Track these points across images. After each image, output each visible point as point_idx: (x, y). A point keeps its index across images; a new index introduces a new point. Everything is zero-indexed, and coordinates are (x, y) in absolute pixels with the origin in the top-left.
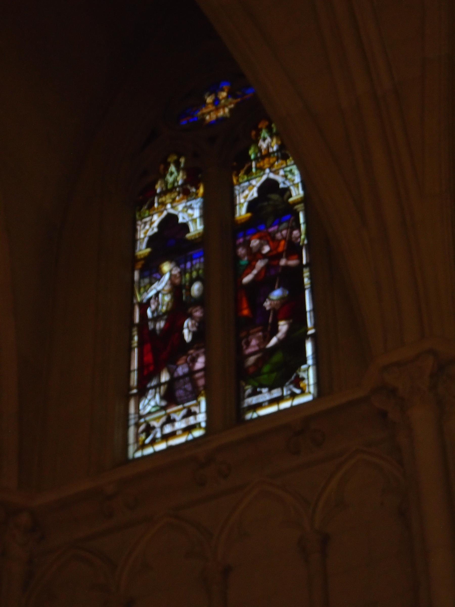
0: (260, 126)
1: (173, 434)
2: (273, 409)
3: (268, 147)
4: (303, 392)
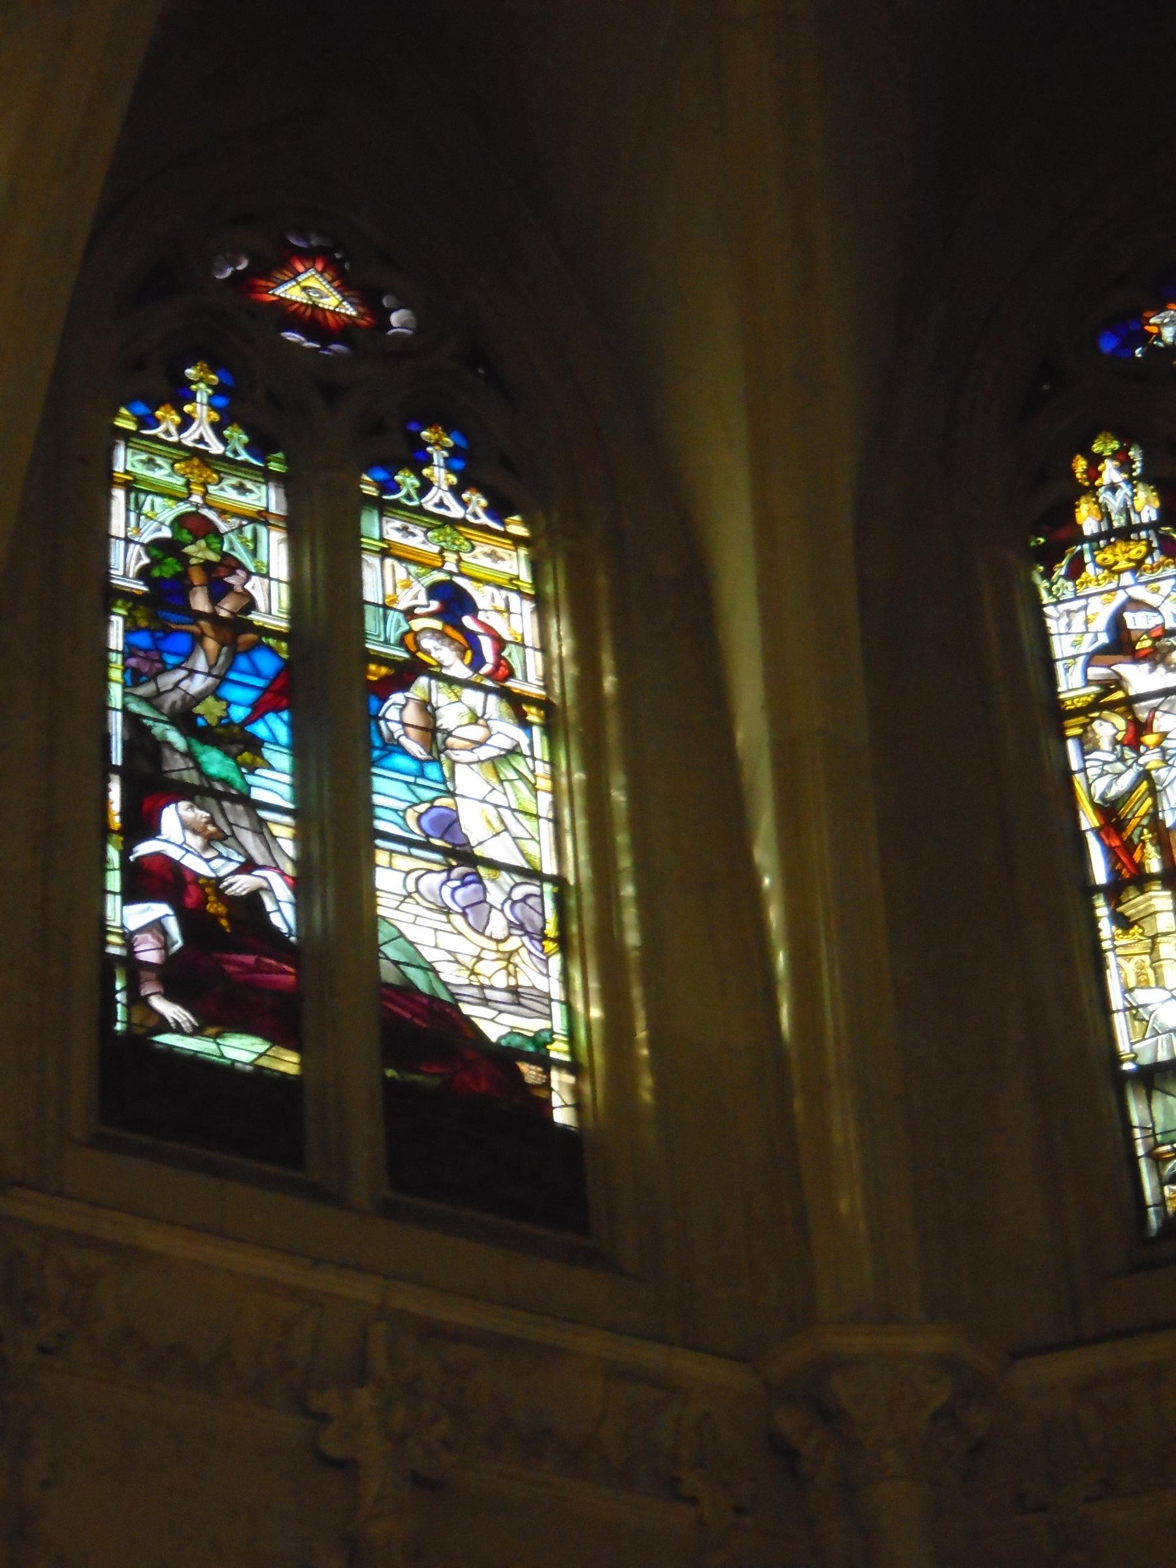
0: (1097, 448)
3: (1126, 511)
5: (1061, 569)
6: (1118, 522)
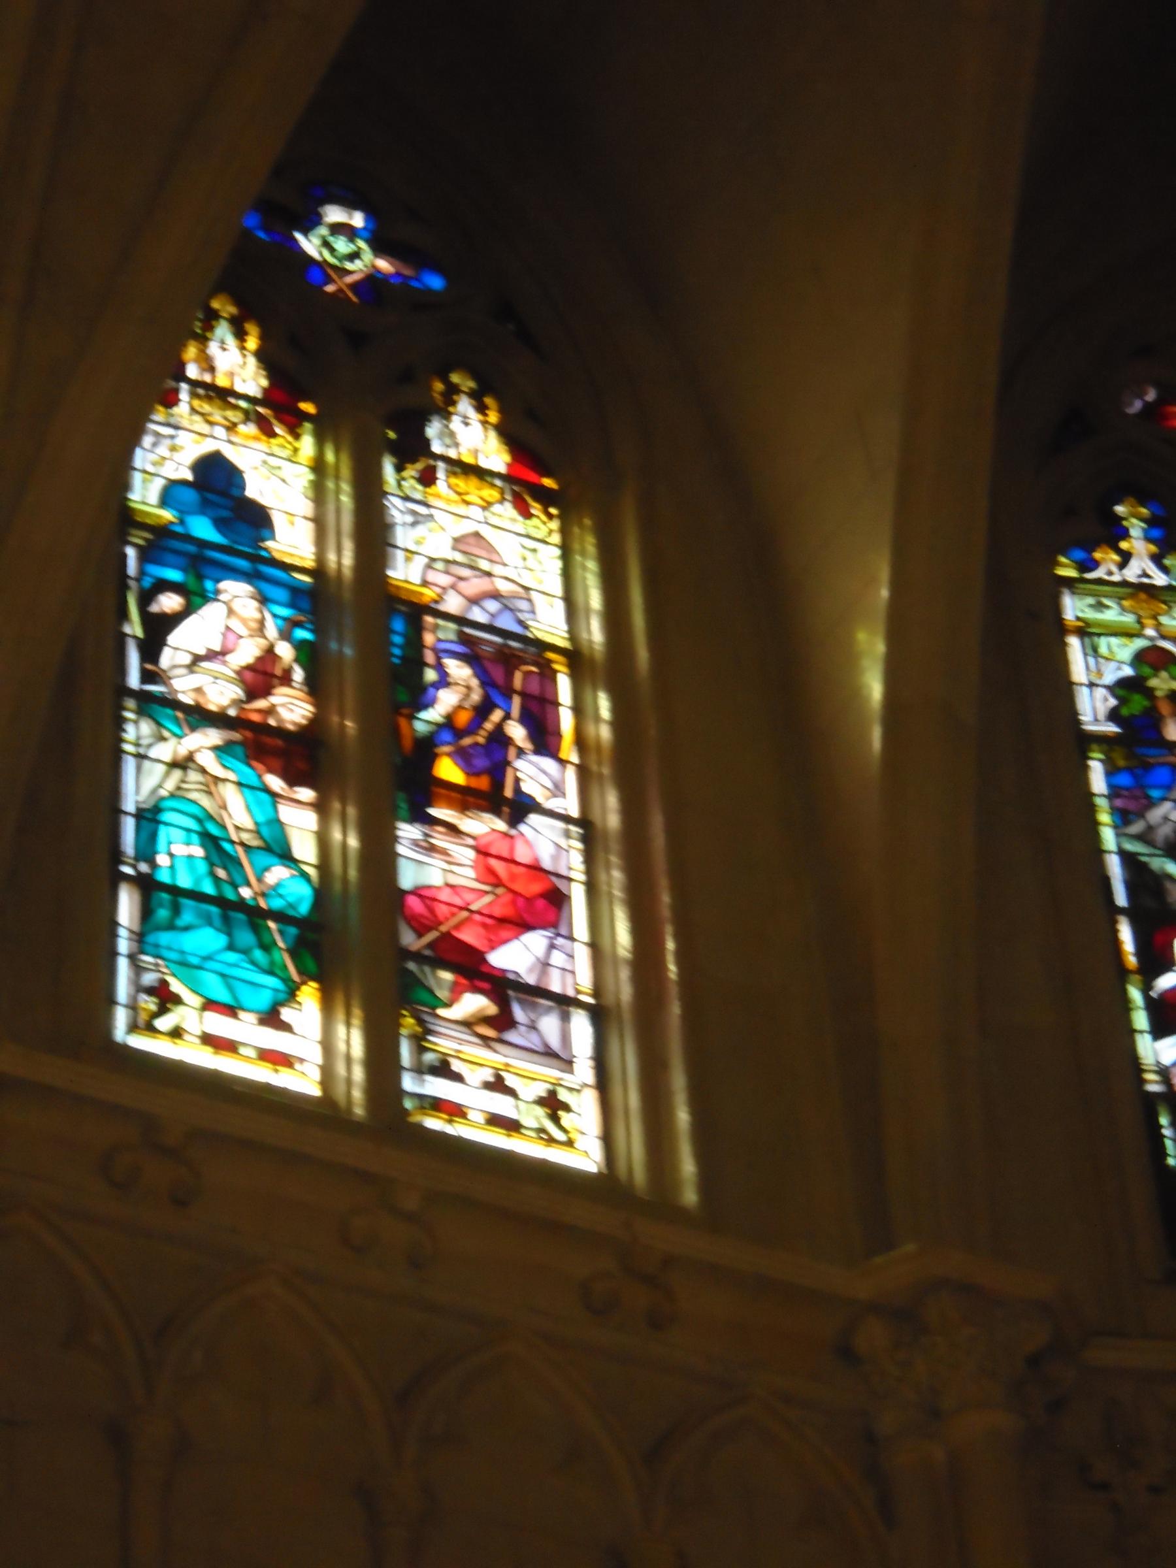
1: (512, 1126)
2: (262, 1074)
4: (570, 1143)
5: (411, 471)
6: (222, 381)
